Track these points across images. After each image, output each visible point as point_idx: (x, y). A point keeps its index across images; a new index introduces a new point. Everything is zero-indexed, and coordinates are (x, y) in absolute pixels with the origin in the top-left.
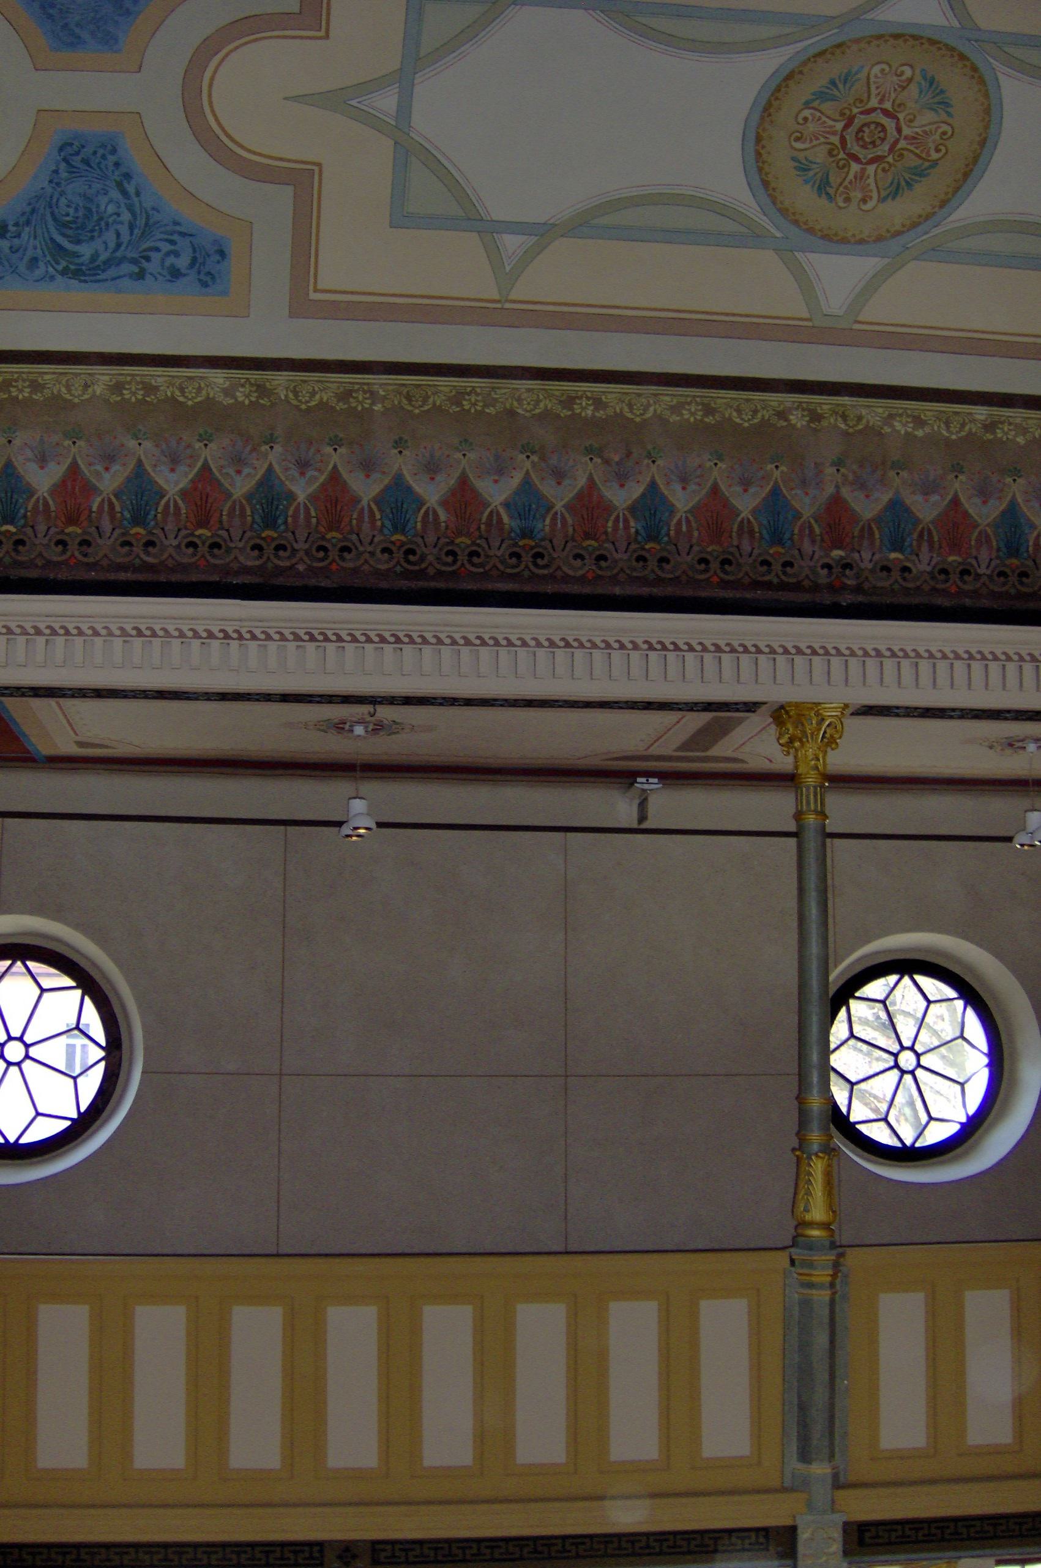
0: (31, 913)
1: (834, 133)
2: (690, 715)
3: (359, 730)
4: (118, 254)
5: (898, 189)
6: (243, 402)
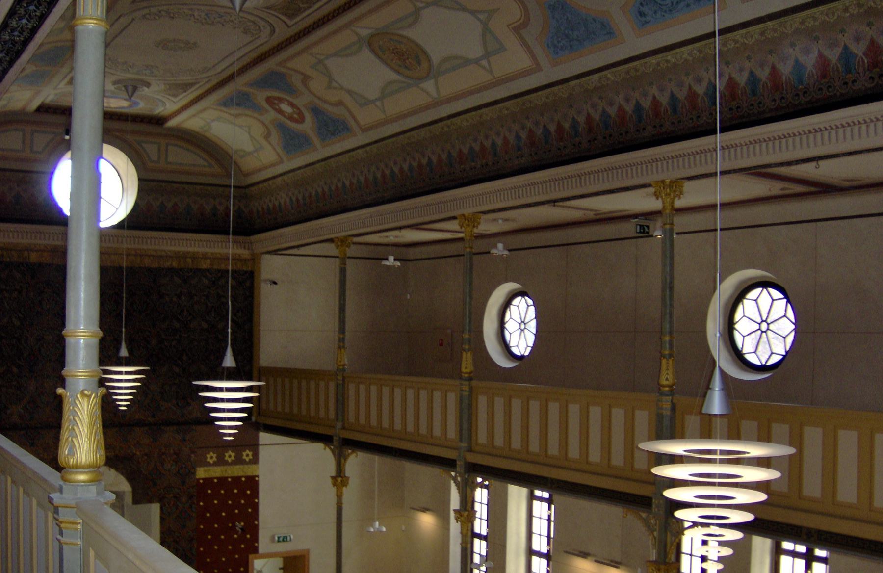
0: (747, 268)
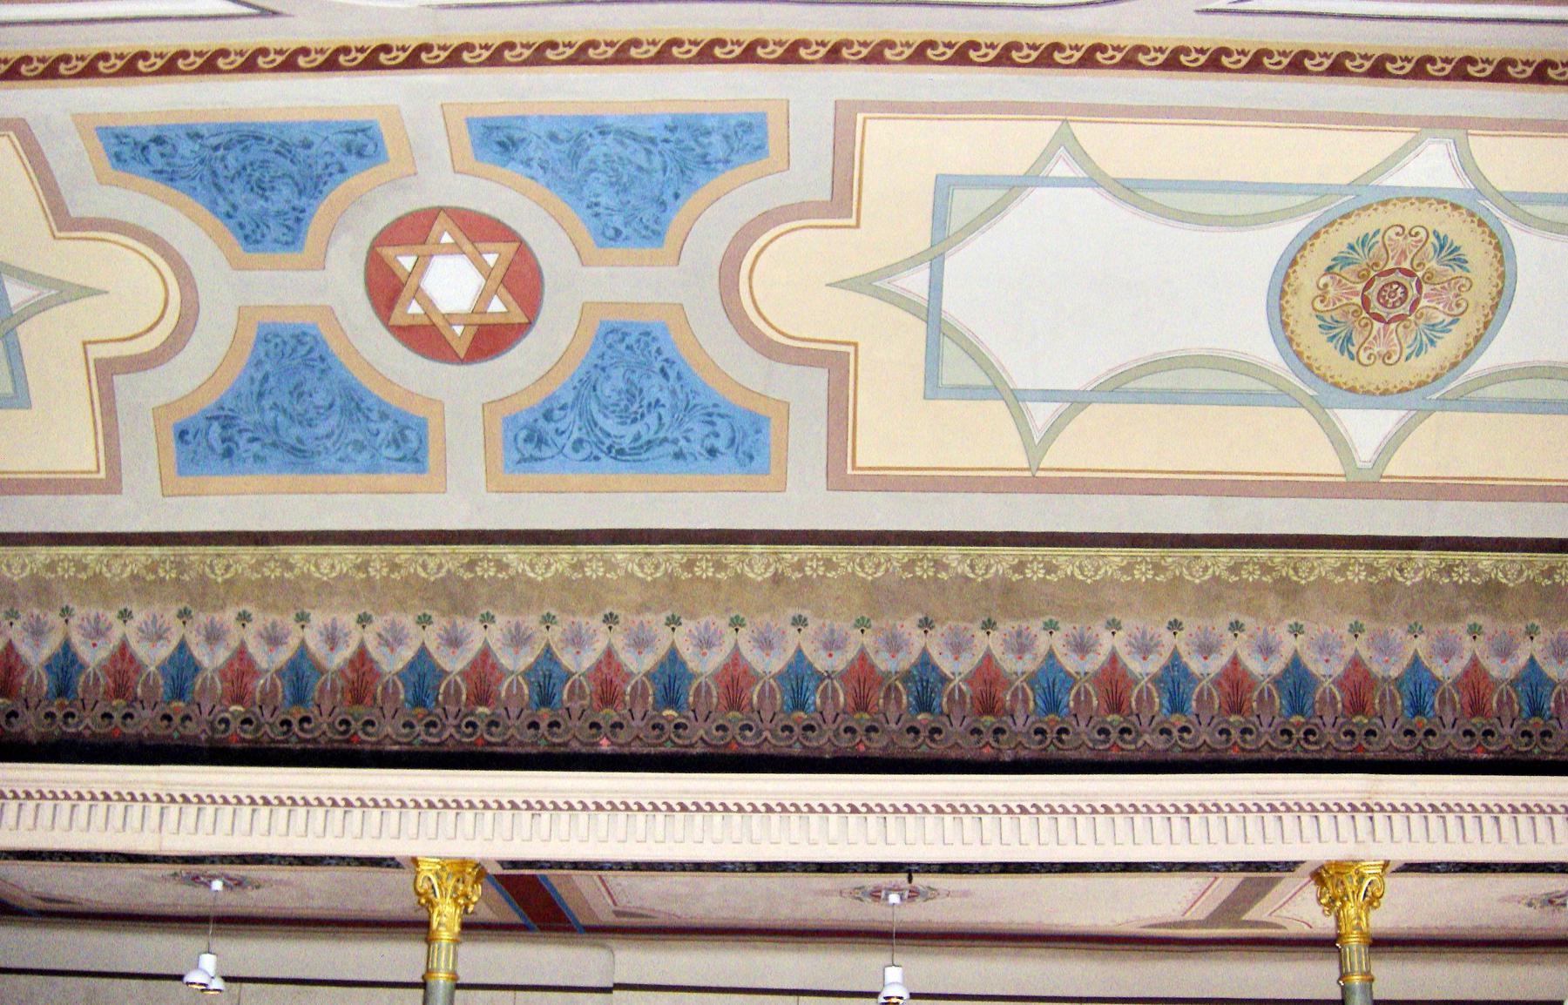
1: (1356, 294)
2: (1222, 876)
3: (894, 898)
4: (661, 435)
5: (1420, 349)
6: (164, 578)
